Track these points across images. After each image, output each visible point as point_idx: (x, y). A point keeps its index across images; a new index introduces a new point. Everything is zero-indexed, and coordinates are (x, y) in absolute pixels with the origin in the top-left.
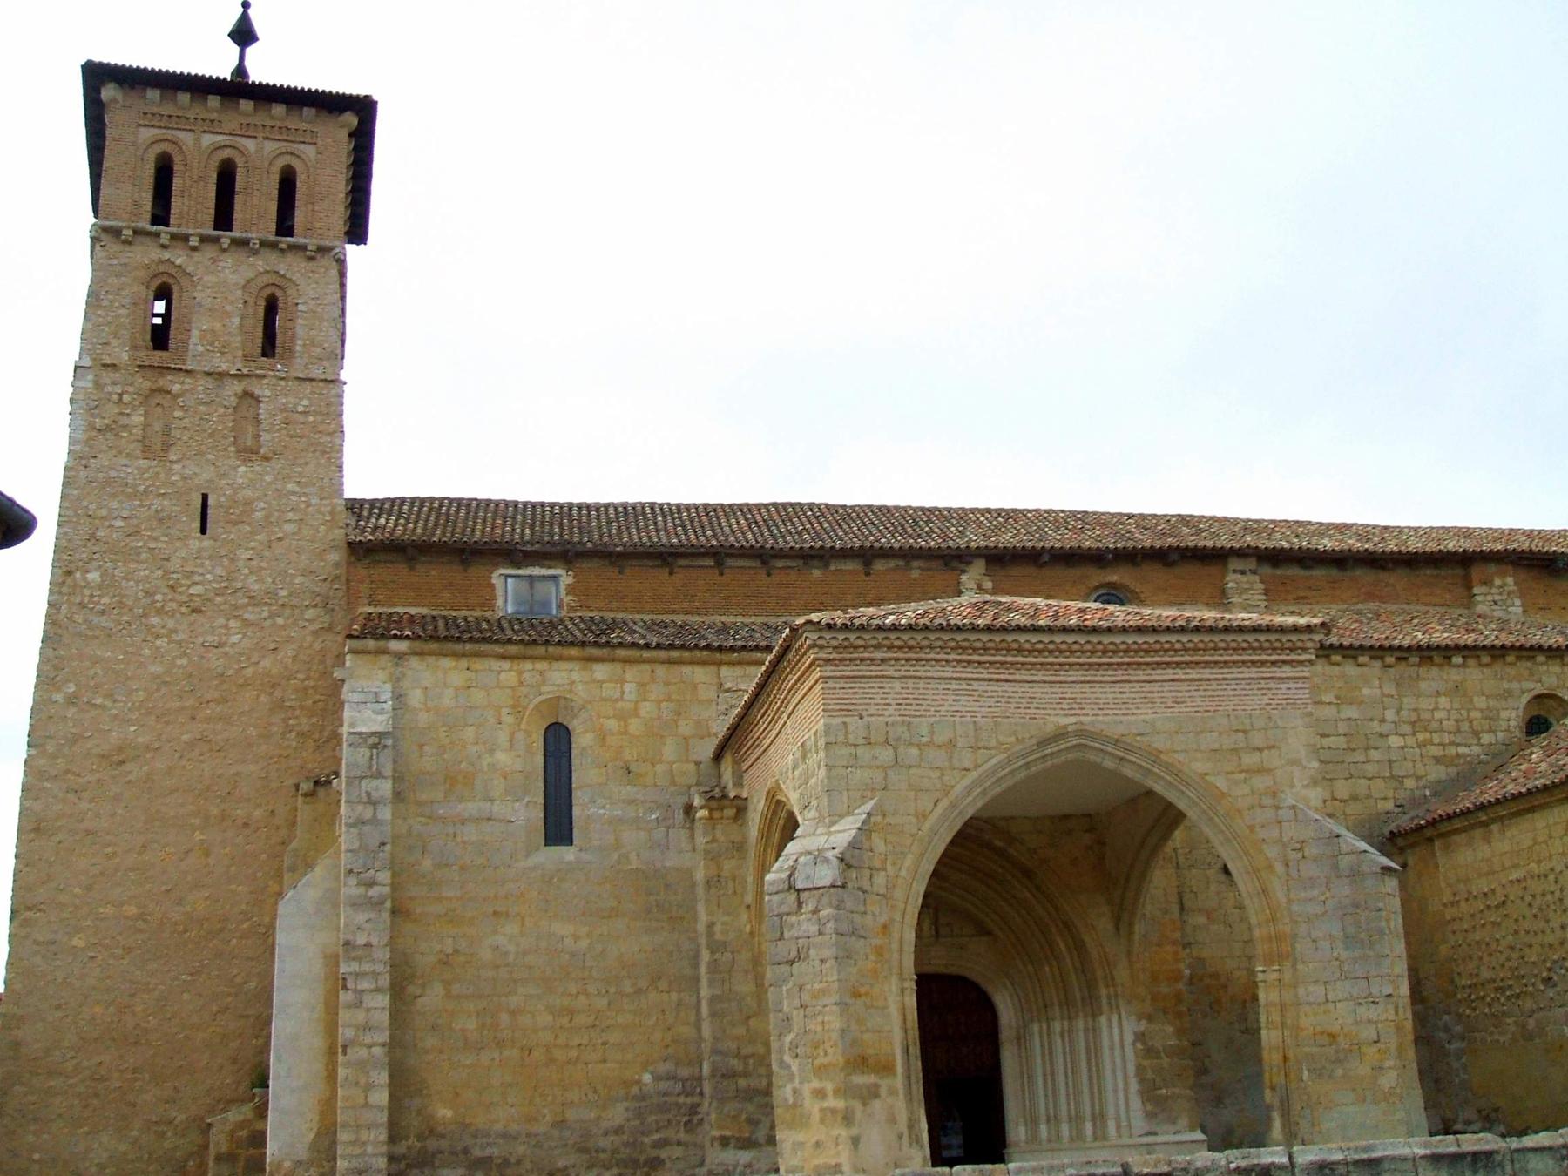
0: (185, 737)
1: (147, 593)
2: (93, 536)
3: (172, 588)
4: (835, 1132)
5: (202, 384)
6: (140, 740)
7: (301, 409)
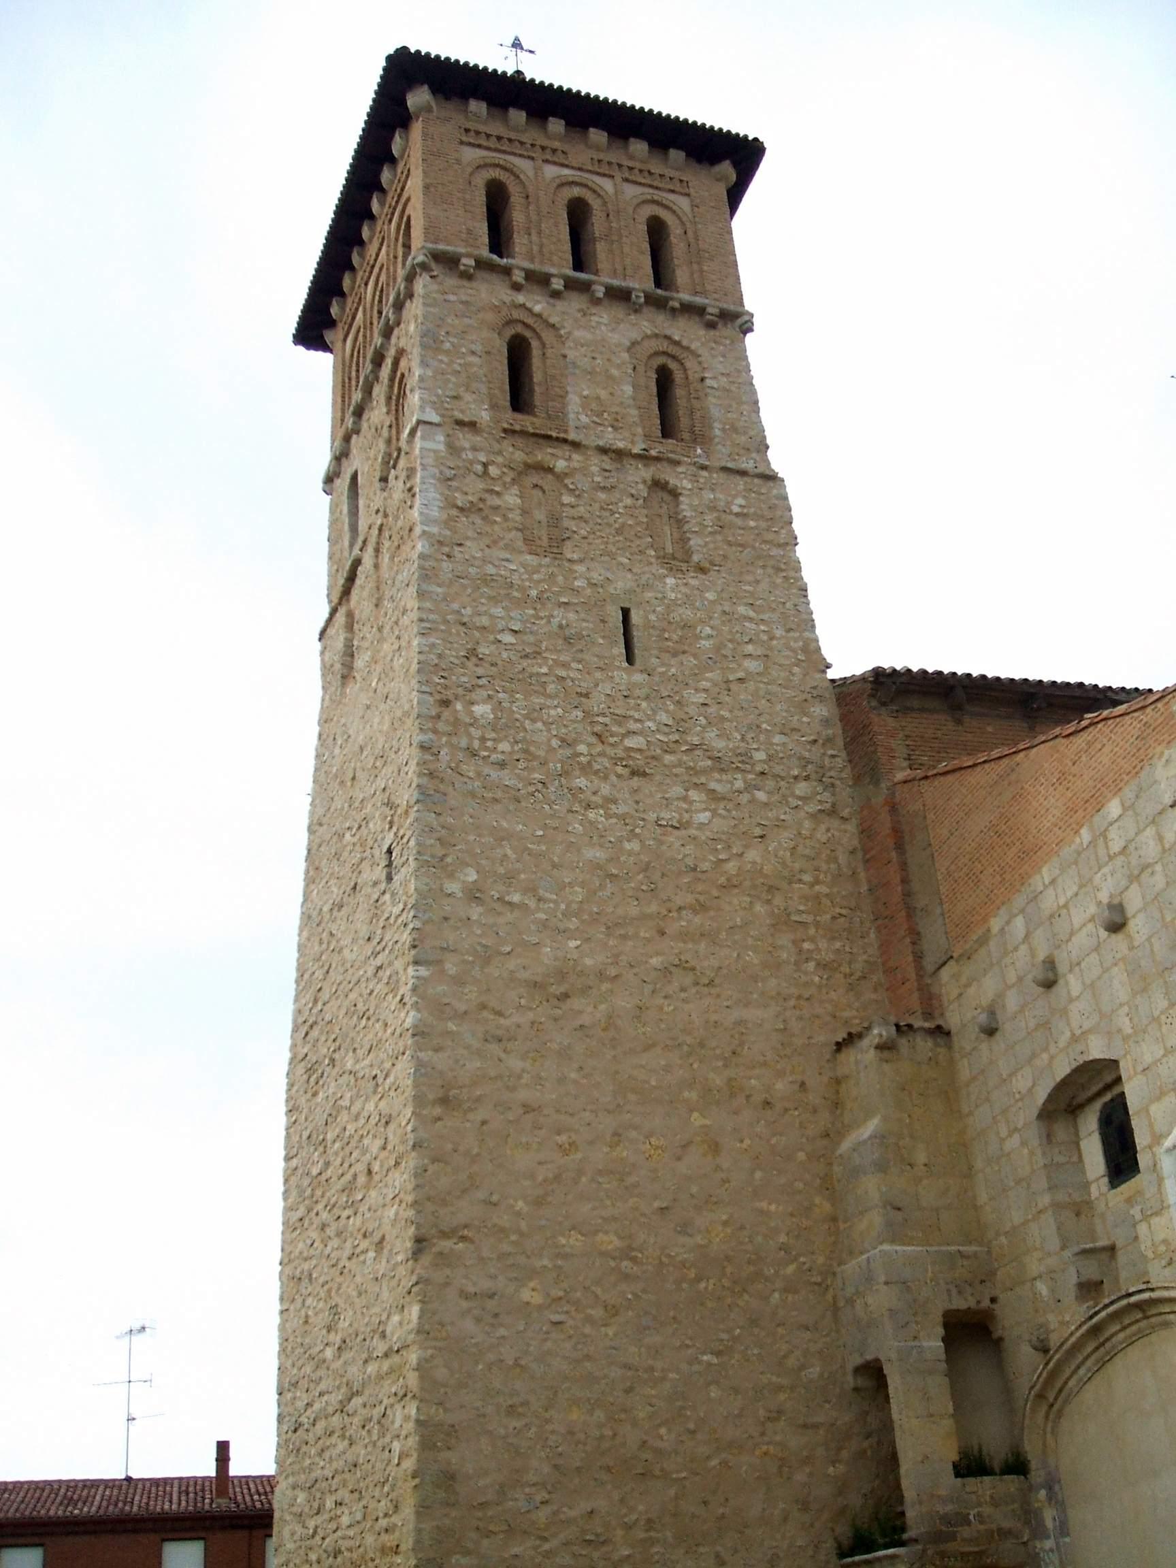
0: (655, 961)
2: (472, 653)
3: (598, 735)
5: (596, 463)
6: (588, 962)
7: (736, 509)
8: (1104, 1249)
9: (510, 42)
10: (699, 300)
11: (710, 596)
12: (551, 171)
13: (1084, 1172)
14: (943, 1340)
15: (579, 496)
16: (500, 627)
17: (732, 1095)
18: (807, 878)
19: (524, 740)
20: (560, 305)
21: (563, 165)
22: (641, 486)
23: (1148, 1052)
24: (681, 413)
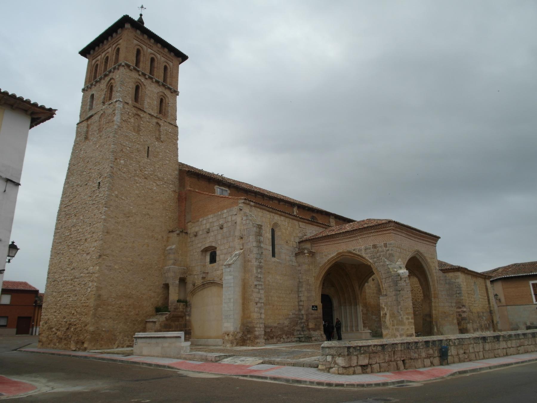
2: (122, 150)
3: (141, 170)
4: (412, 327)
5: (148, 116)
7: (170, 131)
8: (207, 273)
9: (140, 6)
10: (171, 87)
11: (163, 147)
12: (149, 50)
15: (144, 123)
17: (152, 237)
18: (169, 202)
19: (128, 169)
20: (147, 81)
21: (152, 49)
23: (222, 248)
24: (163, 109)
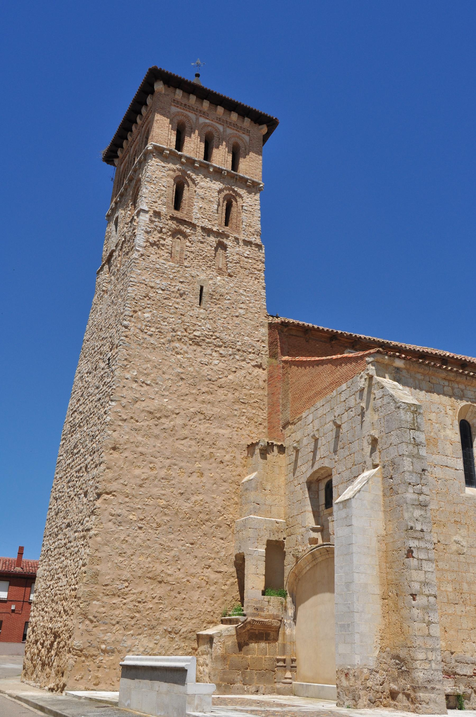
0: (192, 410)
1: (173, 330)
6: (170, 407)
7: (246, 255)
11: (232, 285)
13: (318, 502)
14: (266, 549)
16: (158, 287)
22: (214, 243)
